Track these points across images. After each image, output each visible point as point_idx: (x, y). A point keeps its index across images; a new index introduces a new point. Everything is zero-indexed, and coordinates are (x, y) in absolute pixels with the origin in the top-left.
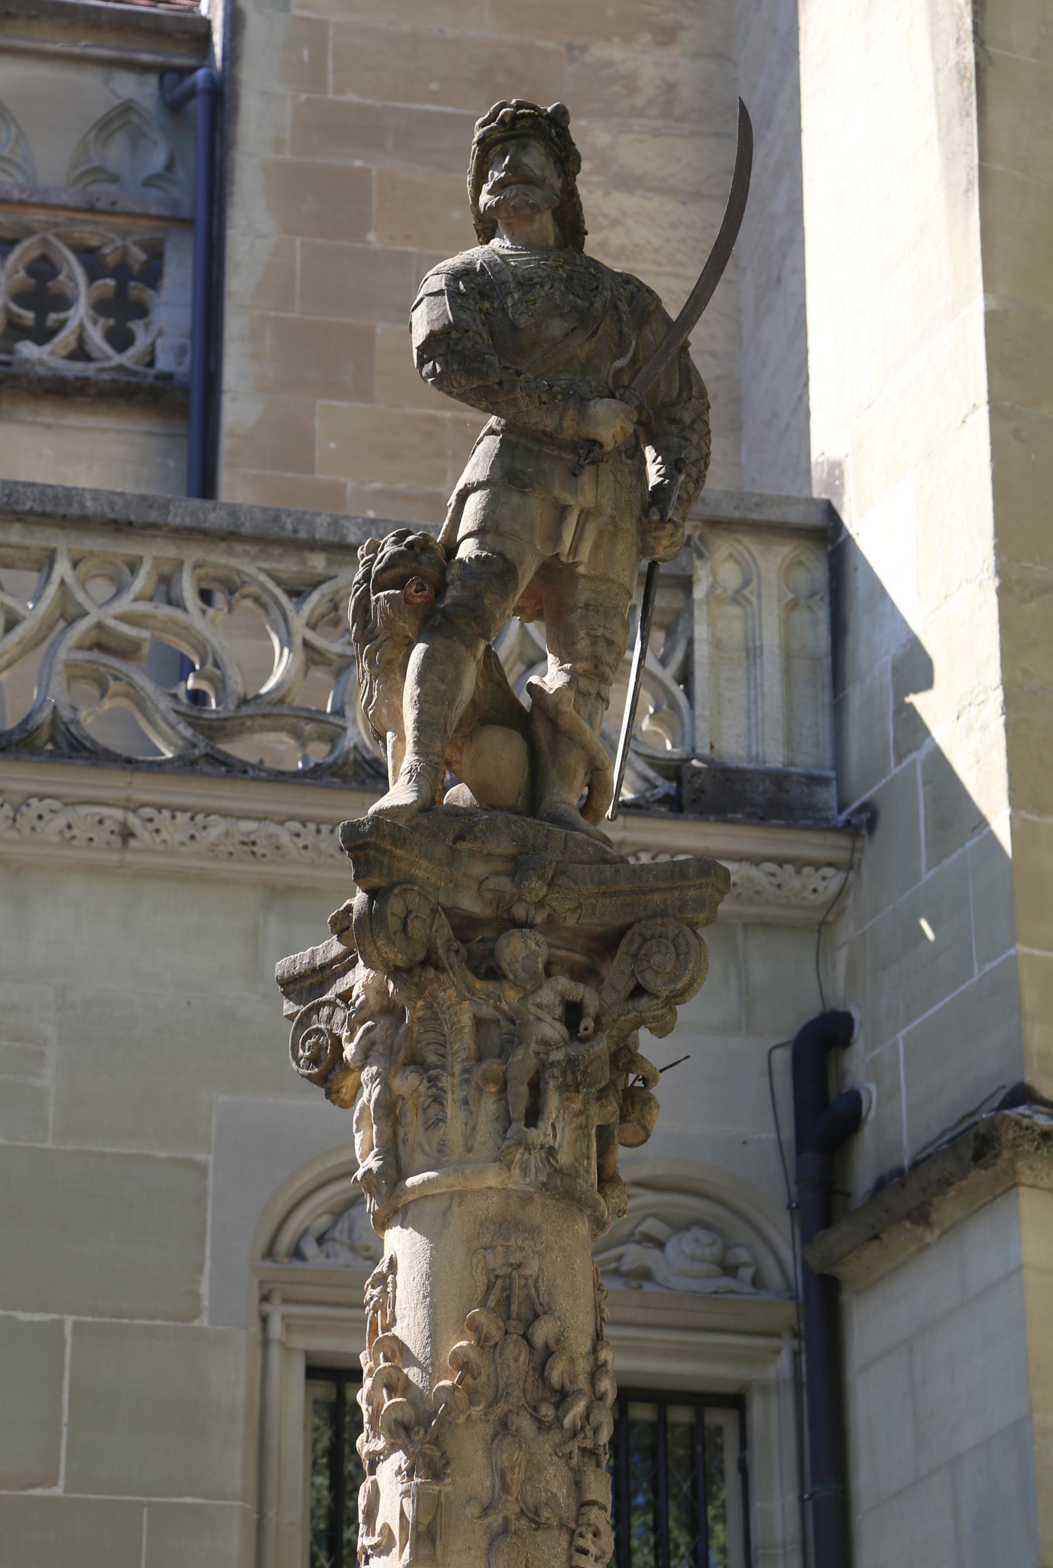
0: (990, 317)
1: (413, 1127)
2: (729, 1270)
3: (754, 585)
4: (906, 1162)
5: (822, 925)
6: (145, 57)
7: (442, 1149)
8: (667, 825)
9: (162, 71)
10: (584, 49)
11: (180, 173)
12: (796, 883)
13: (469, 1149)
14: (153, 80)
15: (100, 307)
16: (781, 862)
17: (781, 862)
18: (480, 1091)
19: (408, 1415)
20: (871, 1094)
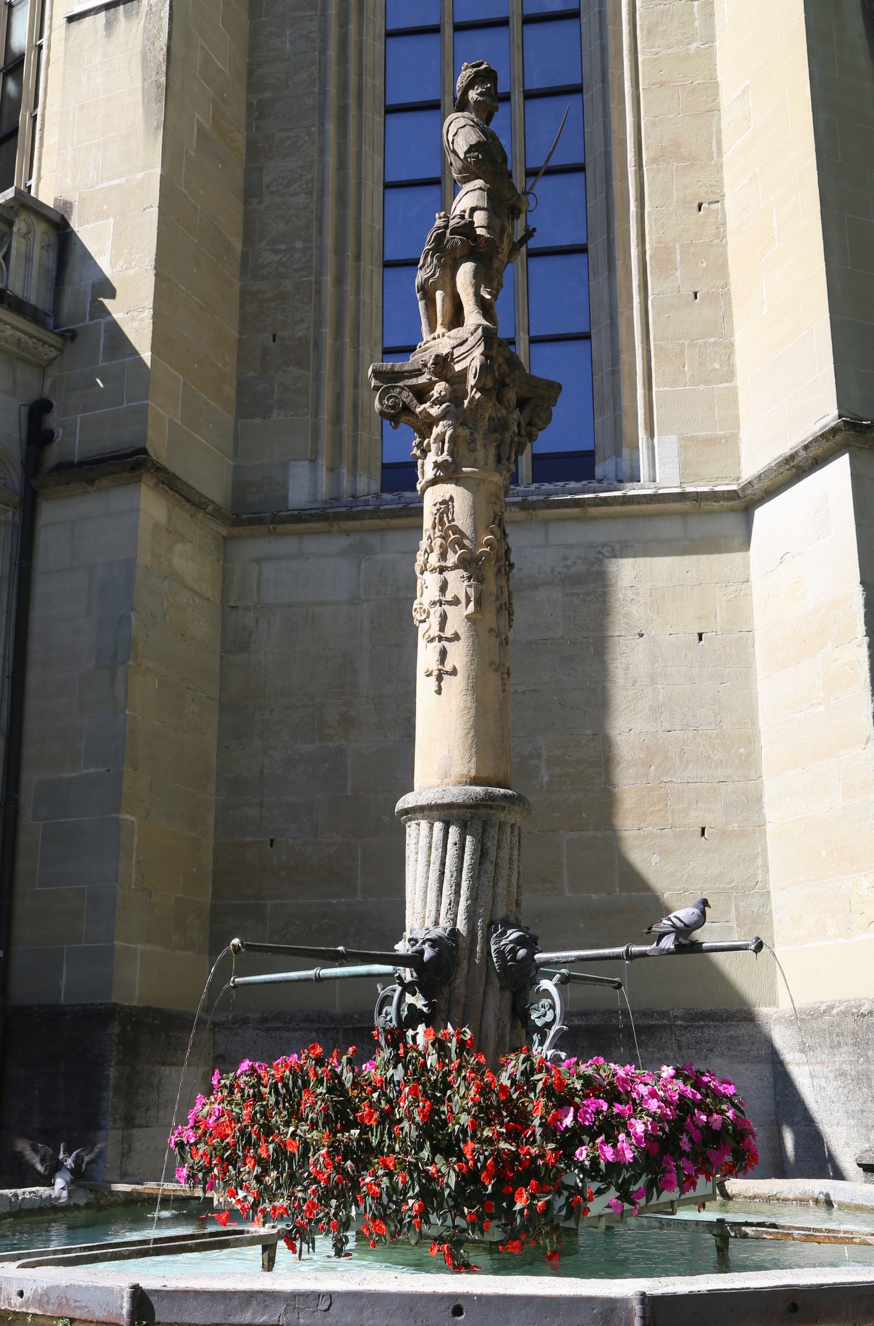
0: (161, 176)
1: (463, 449)
3: (32, 234)
4: (76, 460)
5: (43, 367)
7: (475, 460)
8: (6, 312)
12: (41, 349)
13: (486, 464)
16: (39, 340)
17: (39, 340)
18: (491, 442)
19: (468, 557)
20: (60, 433)
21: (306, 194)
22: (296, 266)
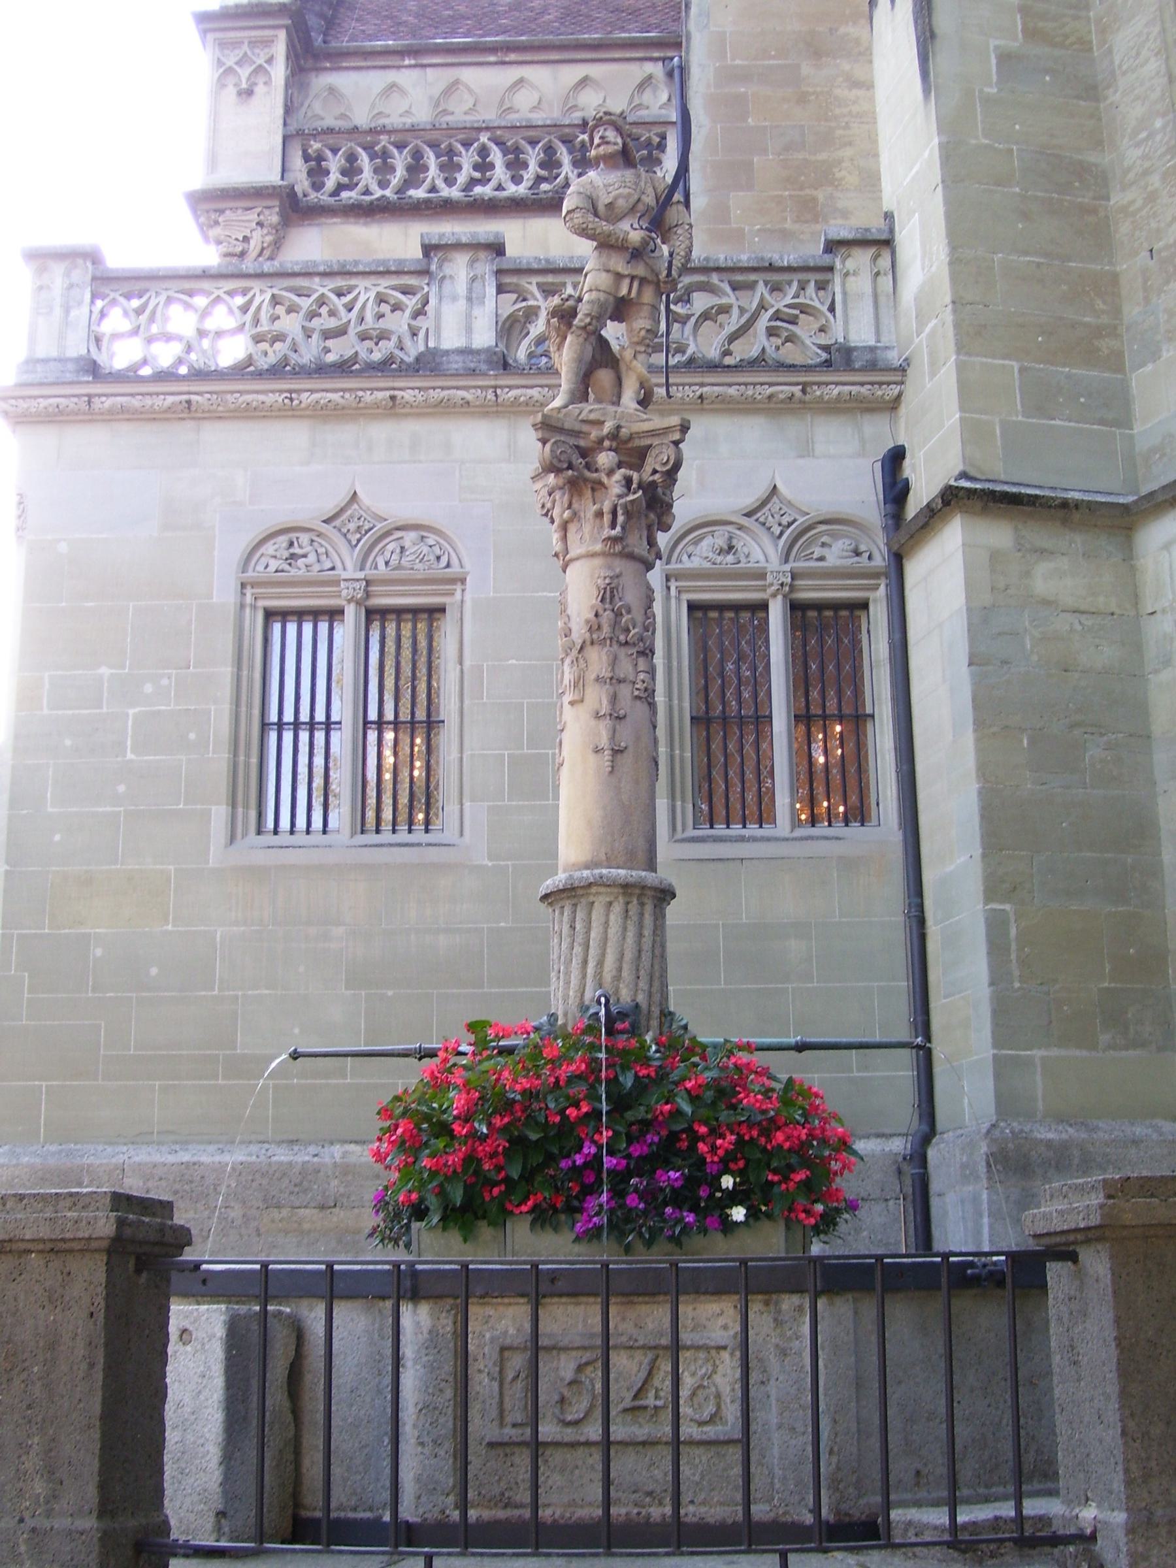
2: (857, 553)
6: (656, 55)
9: (663, 60)
10: (836, 30)
11: (674, 102)
14: (661, 64)
15: (442, 167)
16: (872, 384)
17: (872, 384)
21: (1156, 55)
22: (1159, 153)
